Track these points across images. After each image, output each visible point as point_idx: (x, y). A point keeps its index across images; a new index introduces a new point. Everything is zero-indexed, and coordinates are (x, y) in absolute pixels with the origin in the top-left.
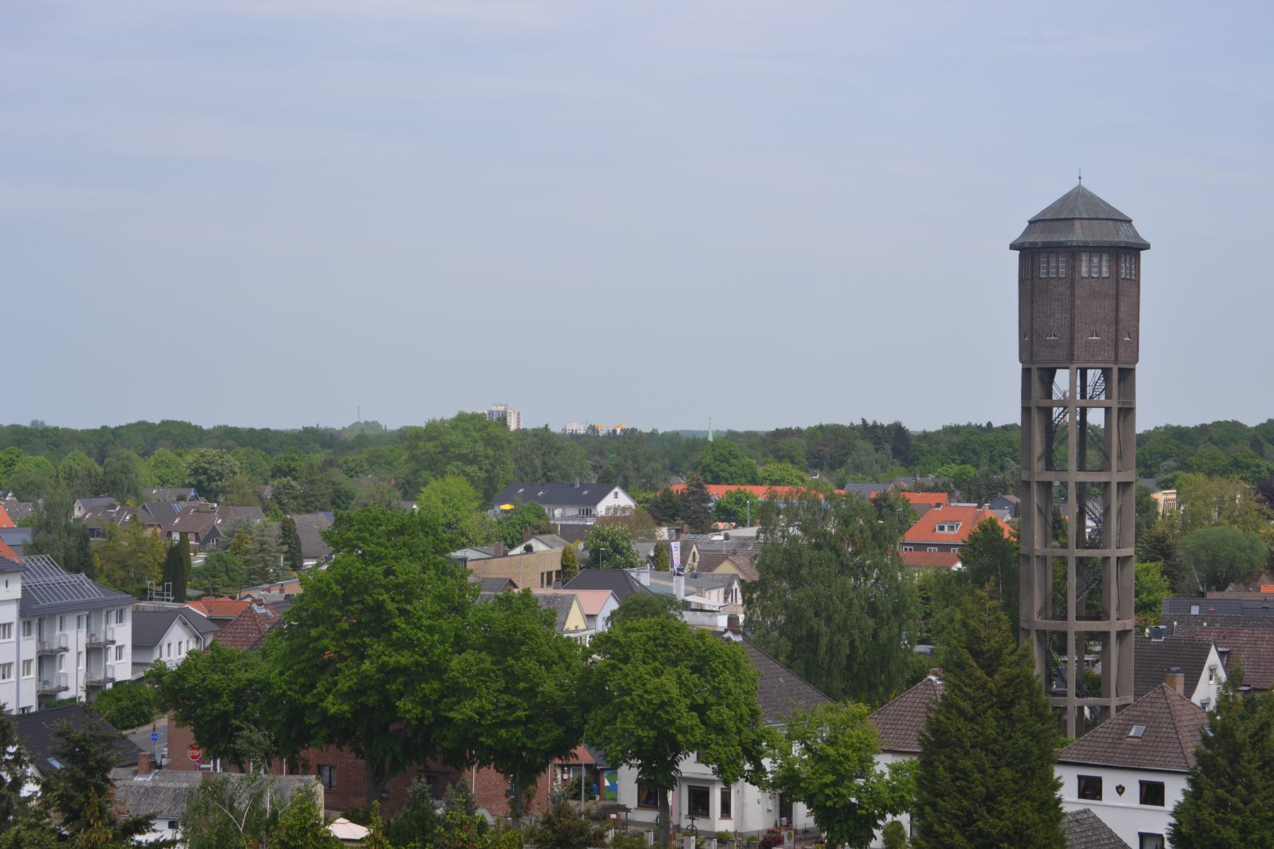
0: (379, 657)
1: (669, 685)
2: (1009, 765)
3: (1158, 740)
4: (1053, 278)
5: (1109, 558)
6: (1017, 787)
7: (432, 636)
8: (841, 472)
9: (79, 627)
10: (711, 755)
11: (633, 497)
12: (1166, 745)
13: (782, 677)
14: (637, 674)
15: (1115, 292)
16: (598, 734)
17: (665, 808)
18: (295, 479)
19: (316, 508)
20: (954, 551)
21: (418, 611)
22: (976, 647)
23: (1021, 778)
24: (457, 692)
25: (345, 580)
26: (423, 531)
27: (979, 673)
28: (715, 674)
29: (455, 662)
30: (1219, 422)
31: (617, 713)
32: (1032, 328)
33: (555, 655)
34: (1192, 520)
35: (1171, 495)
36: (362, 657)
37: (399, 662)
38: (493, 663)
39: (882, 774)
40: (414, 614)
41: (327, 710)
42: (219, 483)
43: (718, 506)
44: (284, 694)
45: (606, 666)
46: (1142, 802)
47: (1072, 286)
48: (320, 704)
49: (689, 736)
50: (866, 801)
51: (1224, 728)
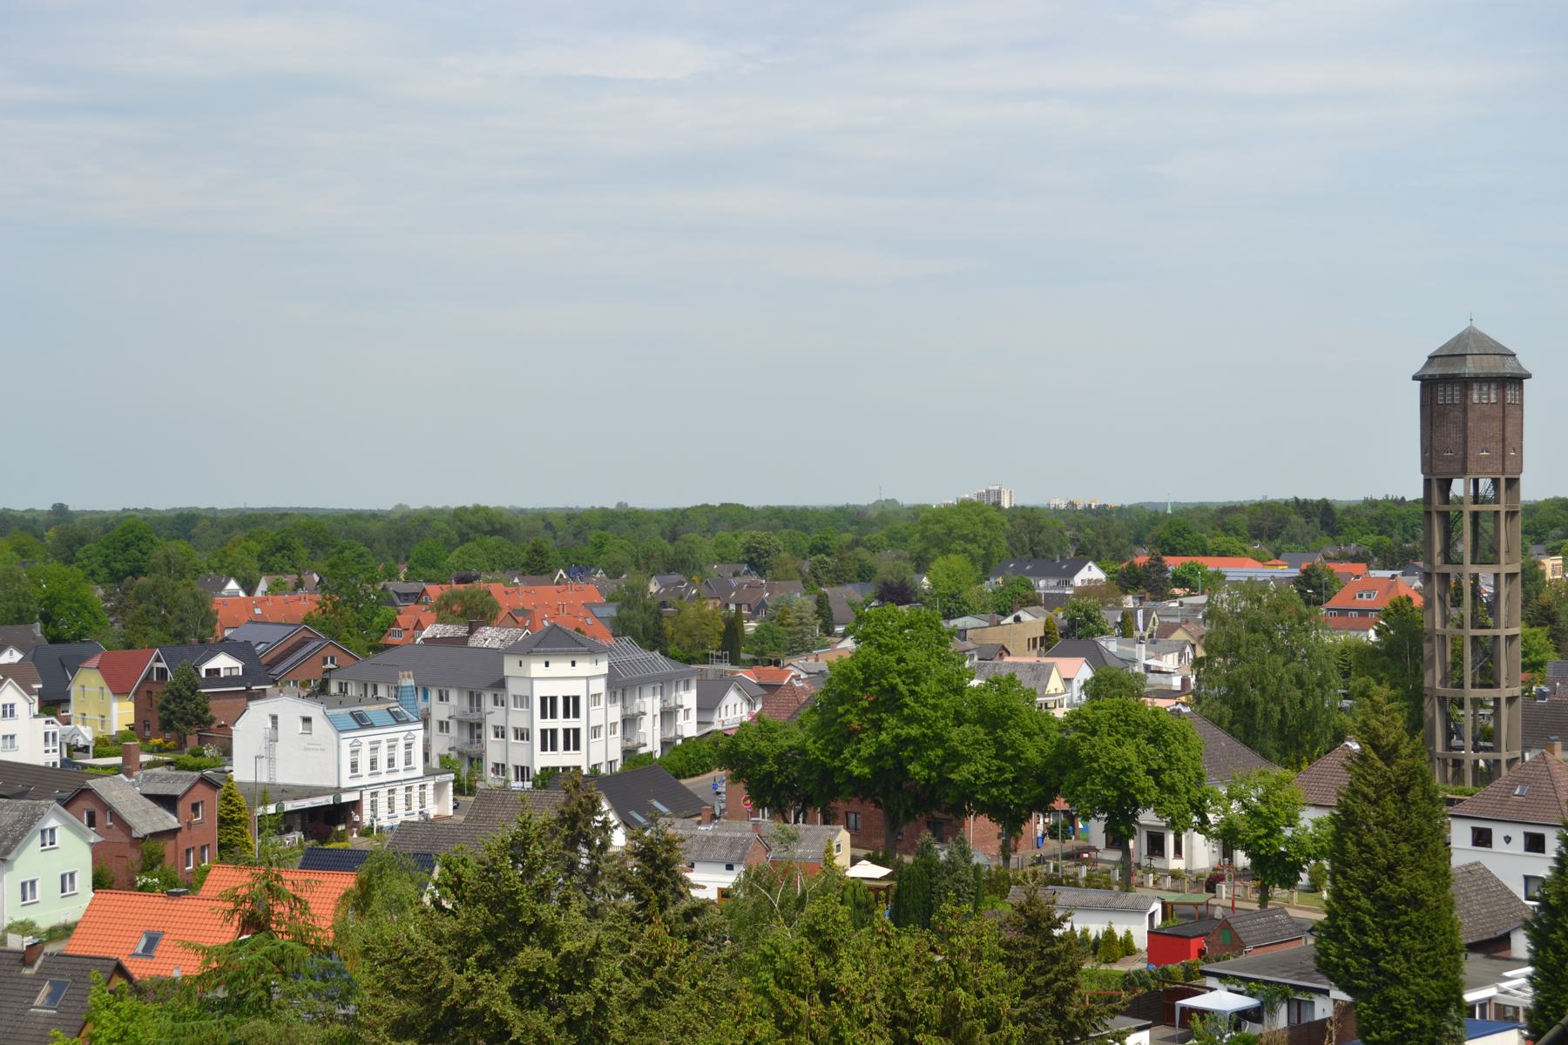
2: (1406, 840)
6: (1412, 858)
7: (936, 712)
8: (1278, 542)
9: (654, 695)
11: (1103, 569)
14: (1103, 745)
16: (1072, 793)
17: (1126, 851)
19: (845, 580)
24: (955, 758)
25: (865, 667)
26: (928, 626)
27: (1379, 764)
28: (1167, 745)
32: (1431, 445)
33: (1036, 727)
35: (1558, 560)
36: (880, 729)
37: (908, 734)
39: (1306, 829)
43: (1174, 575)
44: (818, 758)
47: (1465, 411)
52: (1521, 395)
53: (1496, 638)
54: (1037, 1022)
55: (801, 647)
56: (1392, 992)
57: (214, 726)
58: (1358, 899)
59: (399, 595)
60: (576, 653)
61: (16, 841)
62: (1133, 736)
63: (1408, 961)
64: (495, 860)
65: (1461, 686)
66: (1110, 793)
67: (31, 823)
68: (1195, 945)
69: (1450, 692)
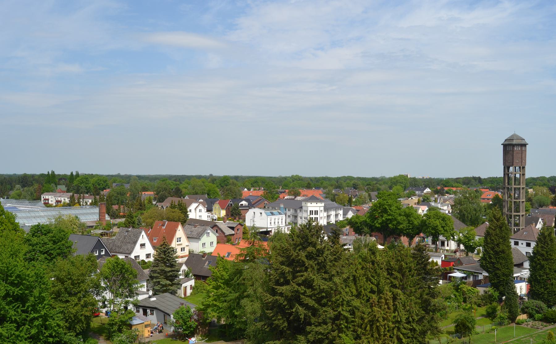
8: (469, 185)
16: (425, 231)
17: (437, 245)
24: (399, 223)
27: (496, 222)
28: (446, 221)
33: (417, 217)
35: (532, 190)
36: (383, 217)
47: (513, 152)
52: (526, 149)
53: (520, 202)
54: (419, 271)
55: (364, 203)
56: (497, 272)
57: (242, 216)
58: (490, 251)
59: (280, 192)
60: (317, 201)
61: (201, 235)
62: (439, 219)
63: (501, 265)
64: (302, 228)
65: (511, 212)
66: (433, 231)
67: (205, 231)
68: (452, 263)
69: (509, 213)
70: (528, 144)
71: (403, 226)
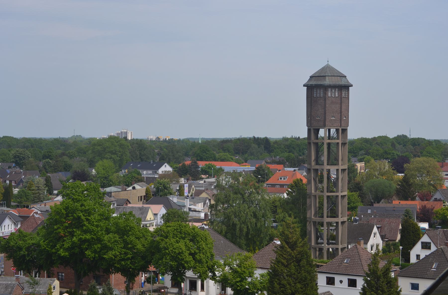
0: (79, 235)
1: (182, 246)
2: (299, 282)
3: (355, 264)
4: (318, 97)
5: (338, 196)
6: (302, 290)
7: (98, 228)
8: (246, 155)
10: (197, 271)
11: (171, 166)
12: (357, 266)
13: (222, 240)
14: (170, 242)
15: (340, 102)
16: (157, 263)
18: (51, 159)
19: (58, 171)
20: (285, 187)
21: (92, 219)
22: (288, 241)
23: (304, 287)
24: (106, 248)
25: (67, 208)
27: (289, 250)
28: (198, 242)
29: (106, 237)
30: (380, 136)
31: (164, 256)
32: (311, 115)
34: (369, 176)
35: (363, 164)
36: (73, 236)
38: (119, 238)
39: (257, 278)
40: (91, 221)
41: (60, 254)
42: (24, 161)
43: (202, 169)
44: (45, 249)
45: (160, 240)
46: (349, 286)
47: (325, 100)
48: (58, 252)
49: (189, 264)
50: (251, 287)
51: (374, 270)
53: (337, 196)
55: (38, 200)
62: (184, 238)
69: (318, 219)
70: (352, 86)
71: (114, 253)
